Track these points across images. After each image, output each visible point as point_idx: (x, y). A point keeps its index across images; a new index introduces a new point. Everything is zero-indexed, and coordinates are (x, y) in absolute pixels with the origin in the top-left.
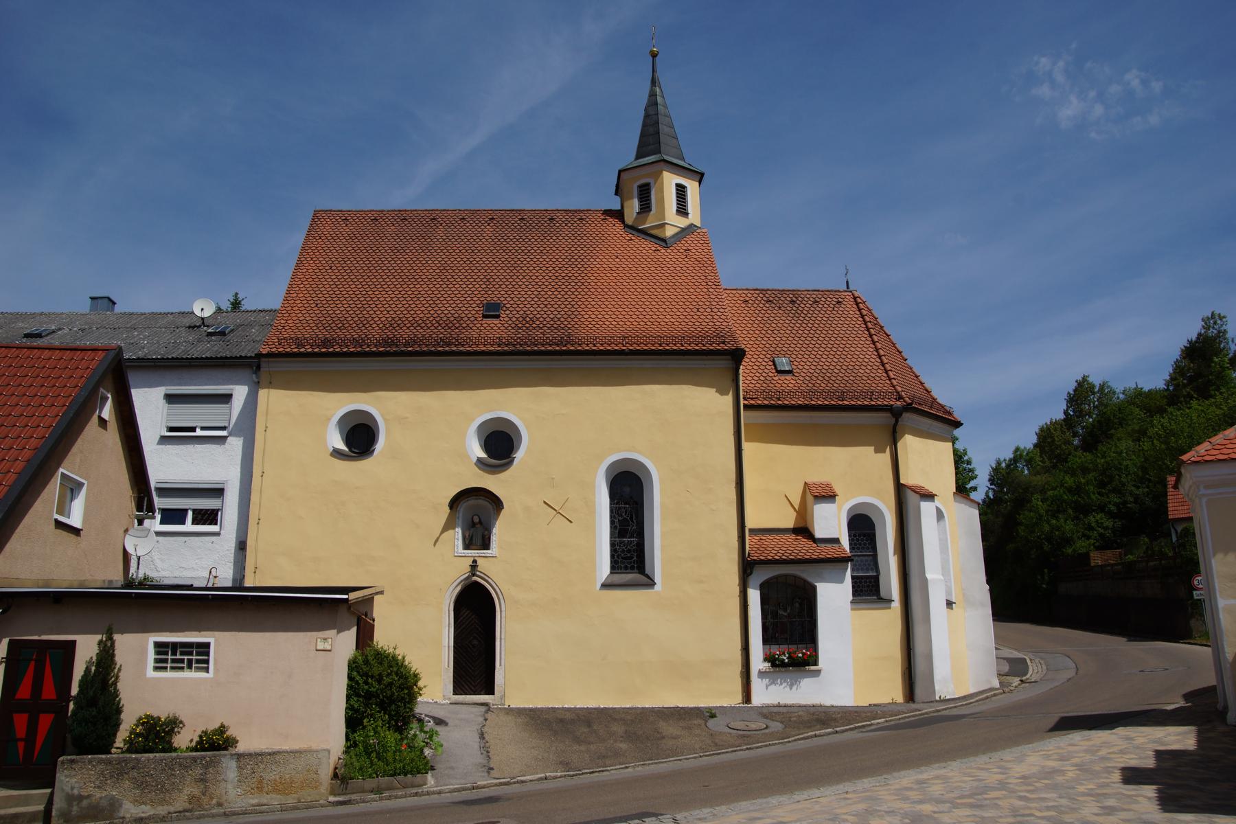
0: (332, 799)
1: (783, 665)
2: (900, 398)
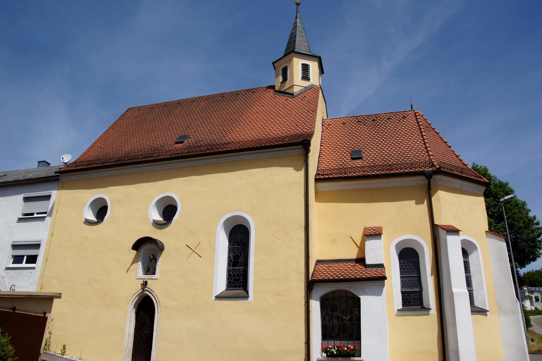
2: (433, 165)
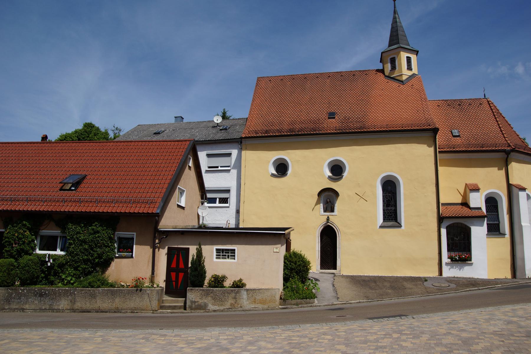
0: (280, 307)
1: (456, 260)
2: (509, 146)
